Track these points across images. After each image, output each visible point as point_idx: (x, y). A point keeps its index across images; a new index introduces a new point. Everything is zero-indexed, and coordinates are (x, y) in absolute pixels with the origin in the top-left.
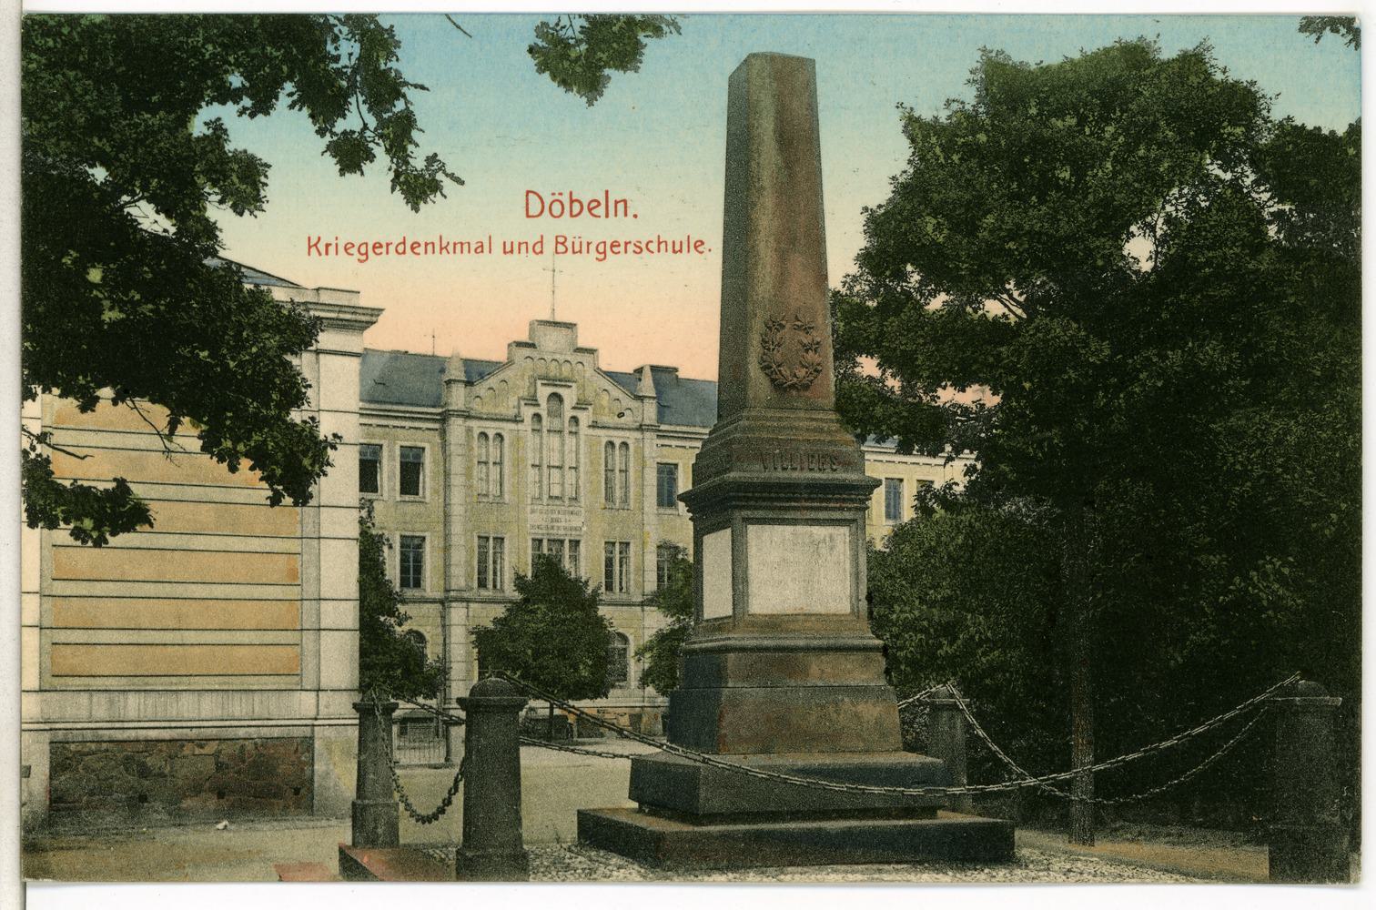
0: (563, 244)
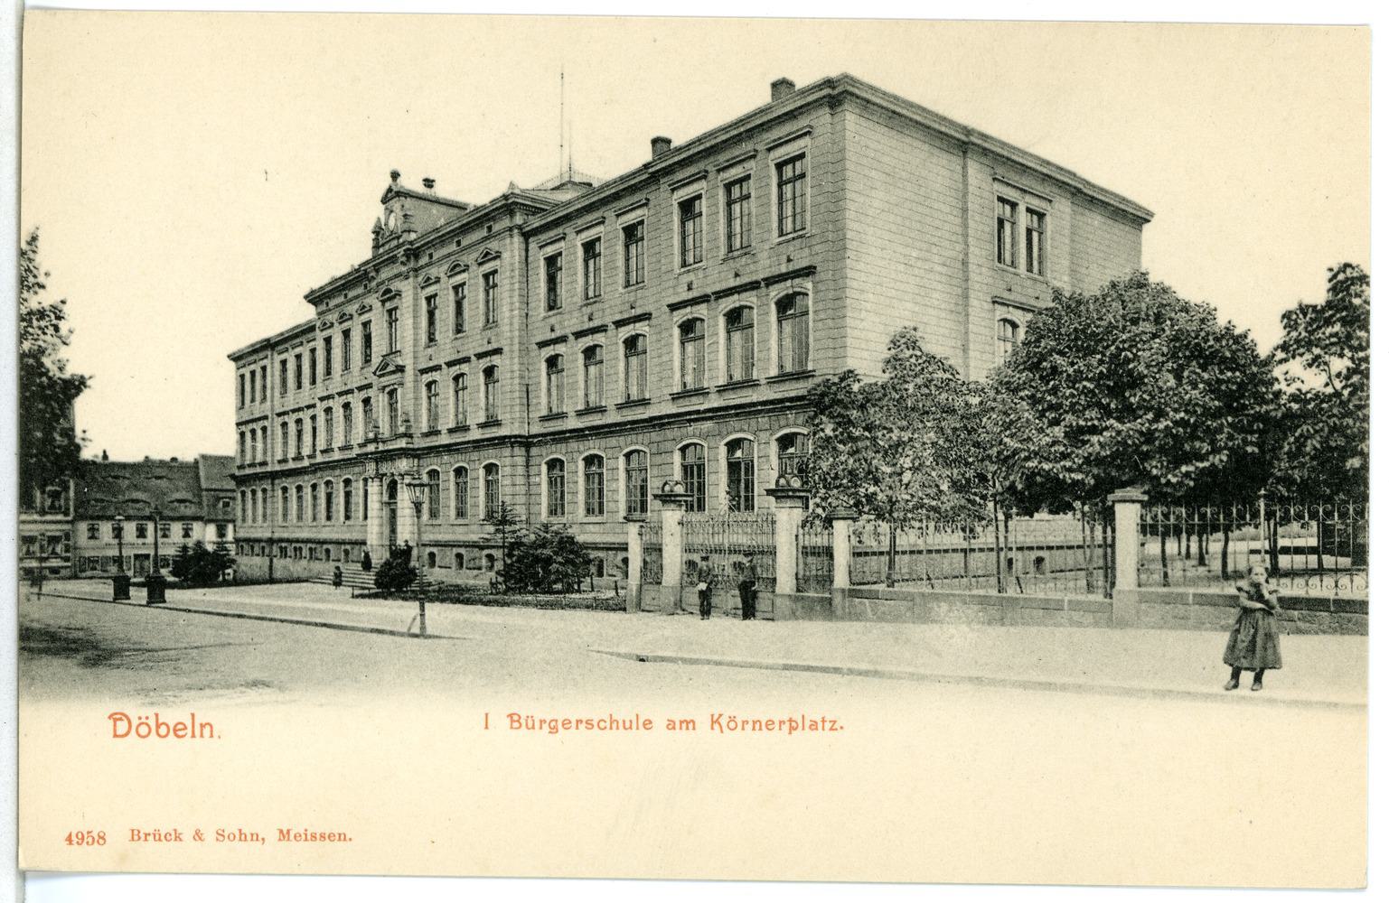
0: (518, 721)
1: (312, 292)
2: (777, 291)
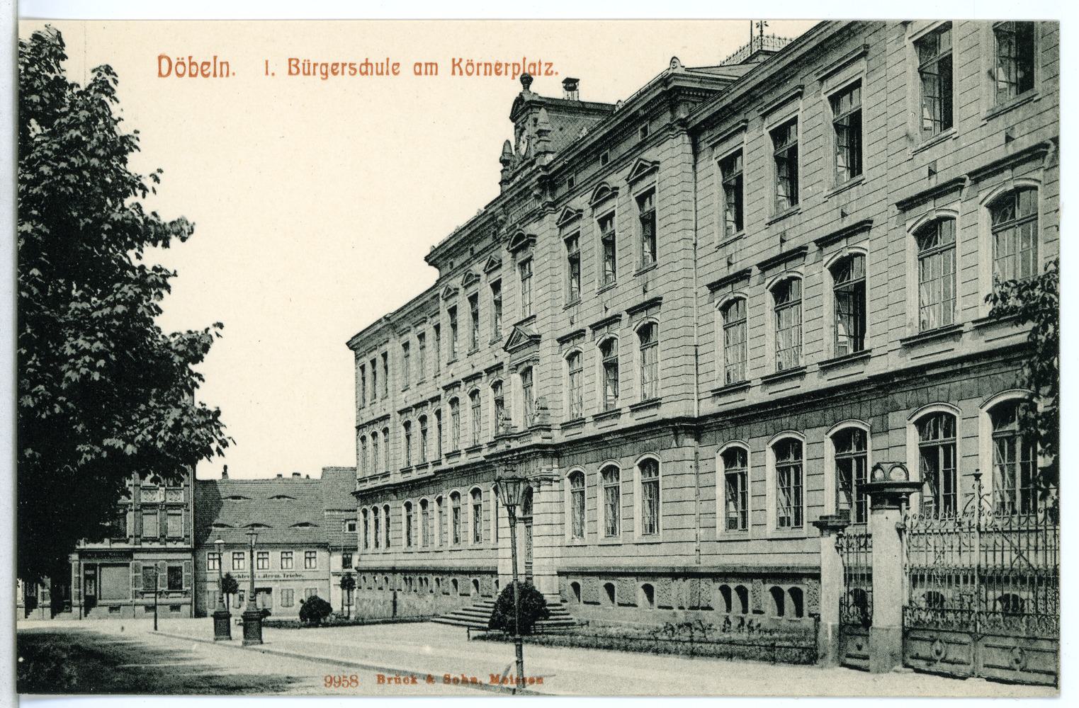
1: (435, 250)
2: (993, 188)
